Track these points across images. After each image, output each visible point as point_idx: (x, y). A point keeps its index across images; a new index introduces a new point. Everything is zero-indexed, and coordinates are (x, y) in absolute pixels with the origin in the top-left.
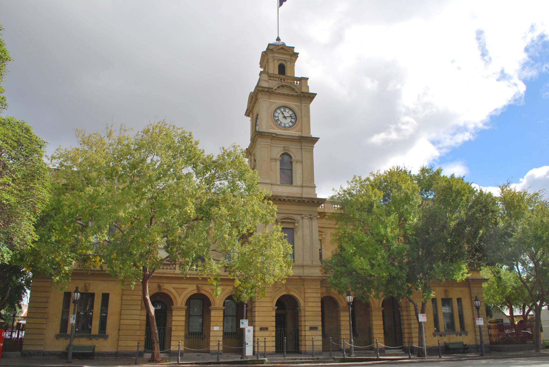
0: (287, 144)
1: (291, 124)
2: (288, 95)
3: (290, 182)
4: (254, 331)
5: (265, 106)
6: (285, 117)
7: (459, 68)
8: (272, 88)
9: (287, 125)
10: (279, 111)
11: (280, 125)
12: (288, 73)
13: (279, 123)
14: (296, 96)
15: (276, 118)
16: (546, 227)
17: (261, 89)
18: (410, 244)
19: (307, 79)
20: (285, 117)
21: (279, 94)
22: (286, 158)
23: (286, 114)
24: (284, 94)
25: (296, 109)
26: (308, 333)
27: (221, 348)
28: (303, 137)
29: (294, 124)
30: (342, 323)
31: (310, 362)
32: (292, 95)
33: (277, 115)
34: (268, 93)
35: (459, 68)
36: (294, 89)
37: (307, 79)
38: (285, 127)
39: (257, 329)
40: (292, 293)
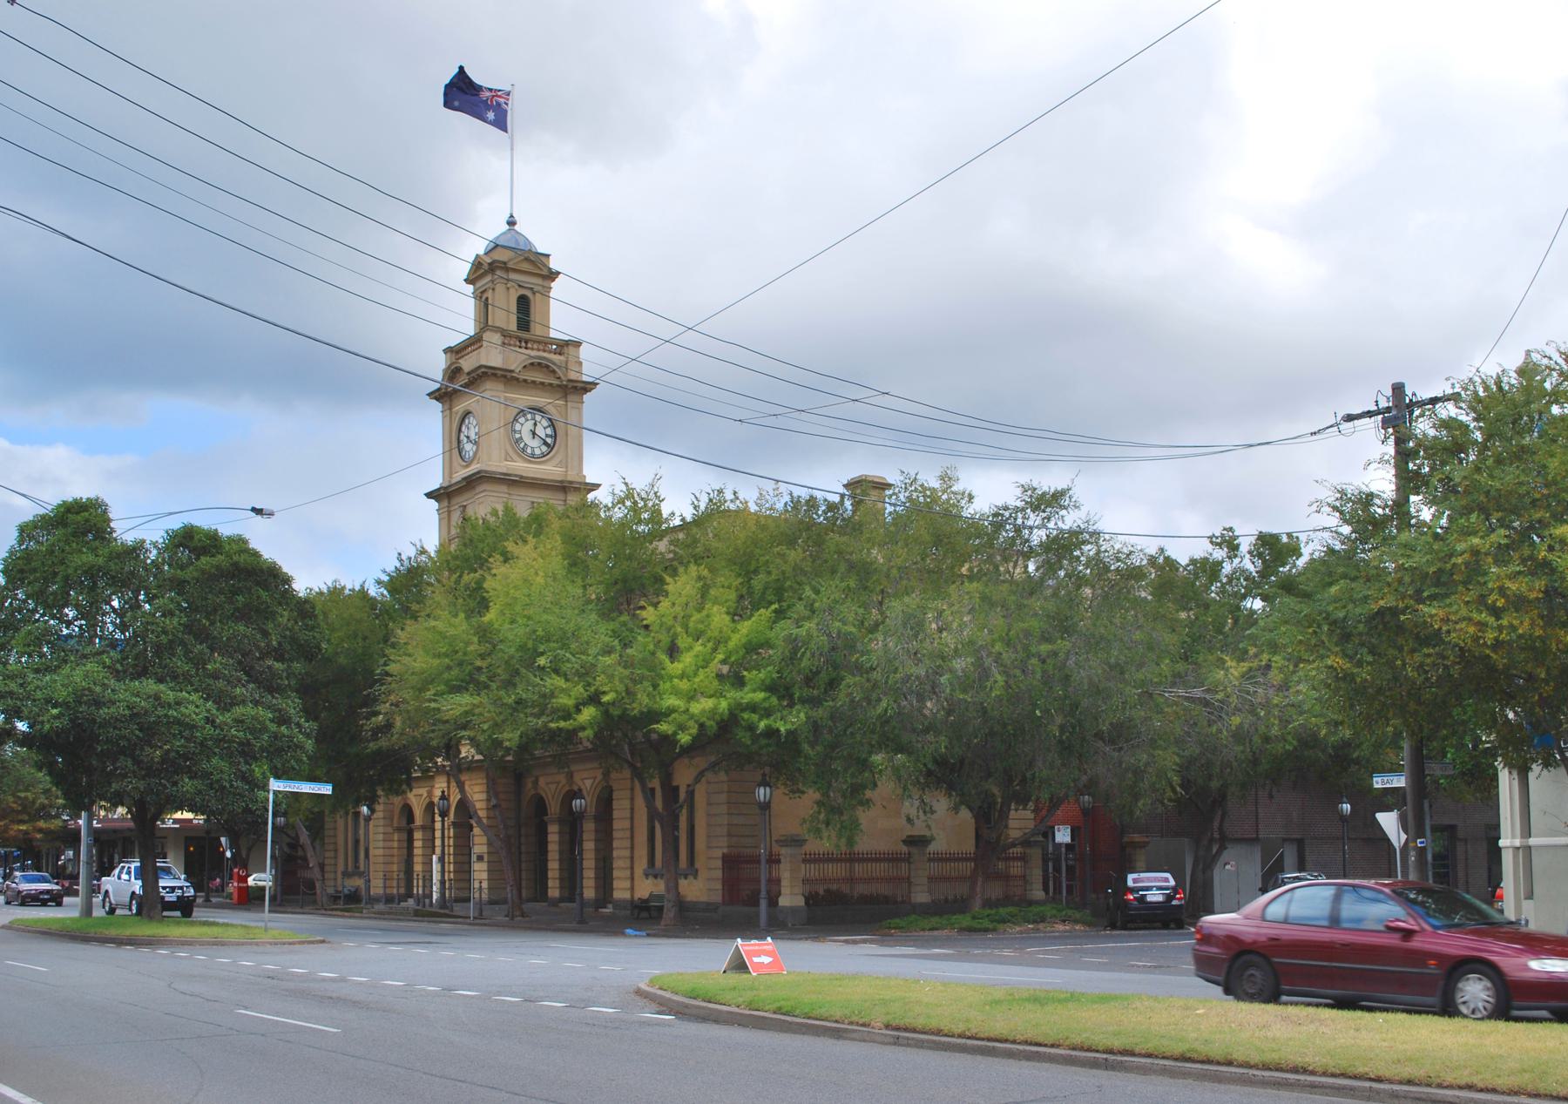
1: (544, 449)
2: (542, 384)
5: (489, 405)
6: (534, 434)
7: (463, 93)
9: (537, 452)
11: (523, 450)
18: (1342, 723)
19: (578, 344)
20: (534, 434)
23: (540, 431)
25: (555, 414)
27: (1506, 781)
29: (551, 447)
30: (585, 882)
33: (518, 427)
35: (463, 93)
36: (554, 372)
37: (578, 344)
38: (533, 456)
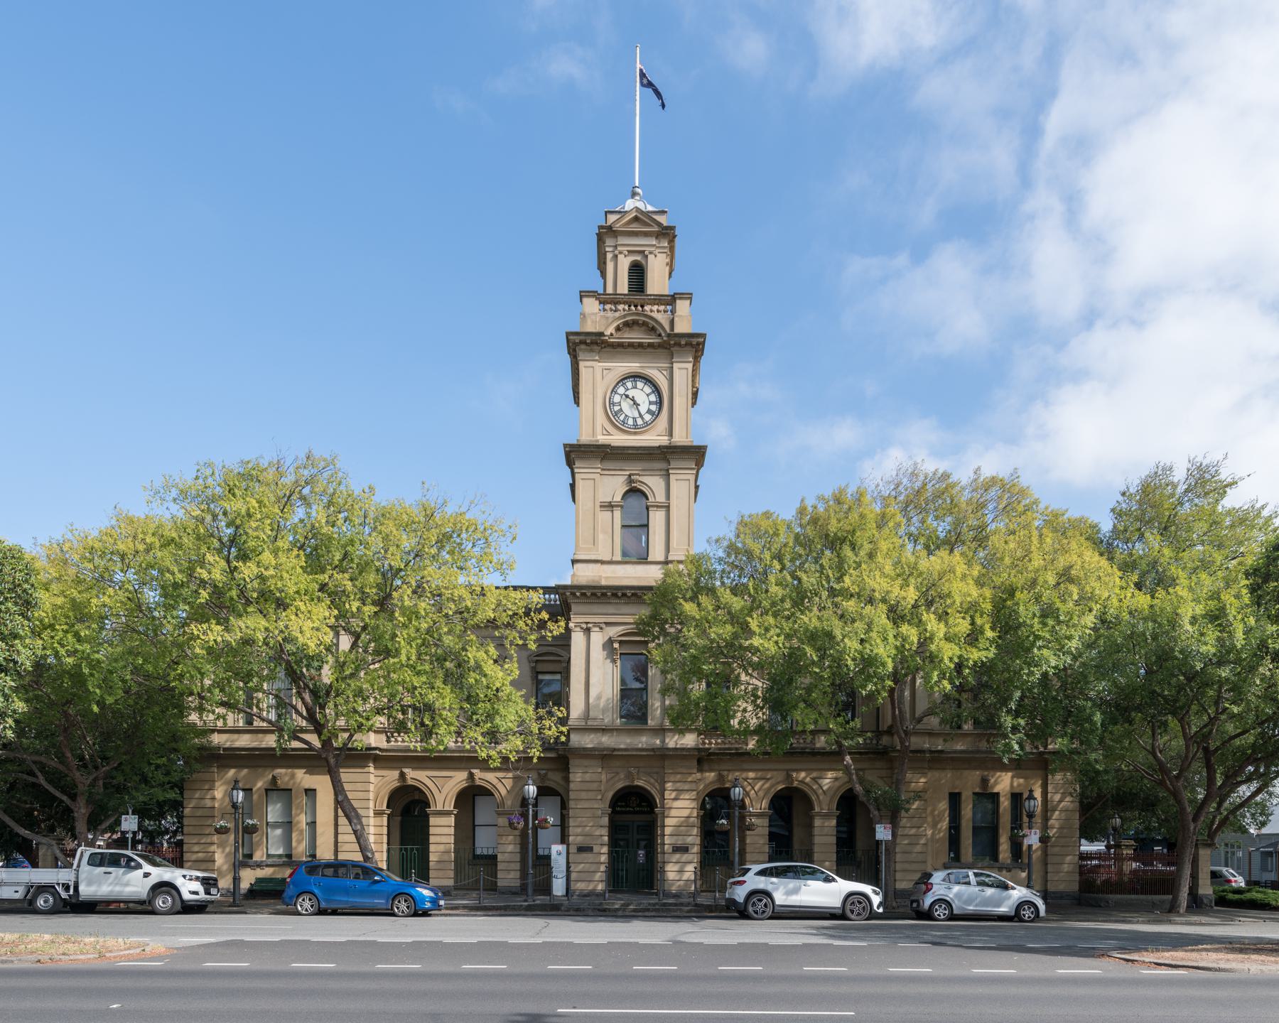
0: (634, 468)
2: (641, 345)
3: (643, 559)
4: (568, 853)
8: (602, 334)
10: (617, 399)
12: (630, 664)
13: (622, 418)
14: (660, 346)
15: (616, 408)
16: (1199, 607)
17: (577, 339)
21: (621, 345)
22: (634, 501)
24: (631, 345)
26: (690, 840)
28: (676, 447)
31: (826, 978)
32: (651, 345)
34: (595, 347)
36: (653, 329)
39: (573, 849)
40: (640, 783)
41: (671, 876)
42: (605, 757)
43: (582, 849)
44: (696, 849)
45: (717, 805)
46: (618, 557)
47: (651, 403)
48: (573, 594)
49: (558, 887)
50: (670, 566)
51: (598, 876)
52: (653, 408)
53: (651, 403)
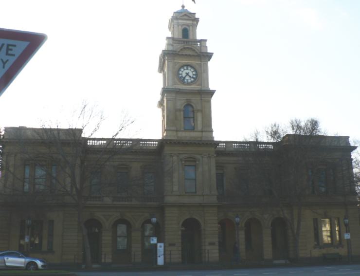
2: (190, 55)
4: (165, 247)
12: (191, 37)
14: (197, 56)
21: (182, 55)
24: (186, 55)
32: (193, 56)
36: (194, 50)
41: (42, 187)
42: (181, 206)
43: (171, 245)
44: (217, 244)
45: (225, 226)
46: (183, 129)
47: (192, 72)
48: (166, 142)
49: (160, 261)
50: (204, 133)
51: (262, 139)
52: (194, 73)
53: (192, 72)
